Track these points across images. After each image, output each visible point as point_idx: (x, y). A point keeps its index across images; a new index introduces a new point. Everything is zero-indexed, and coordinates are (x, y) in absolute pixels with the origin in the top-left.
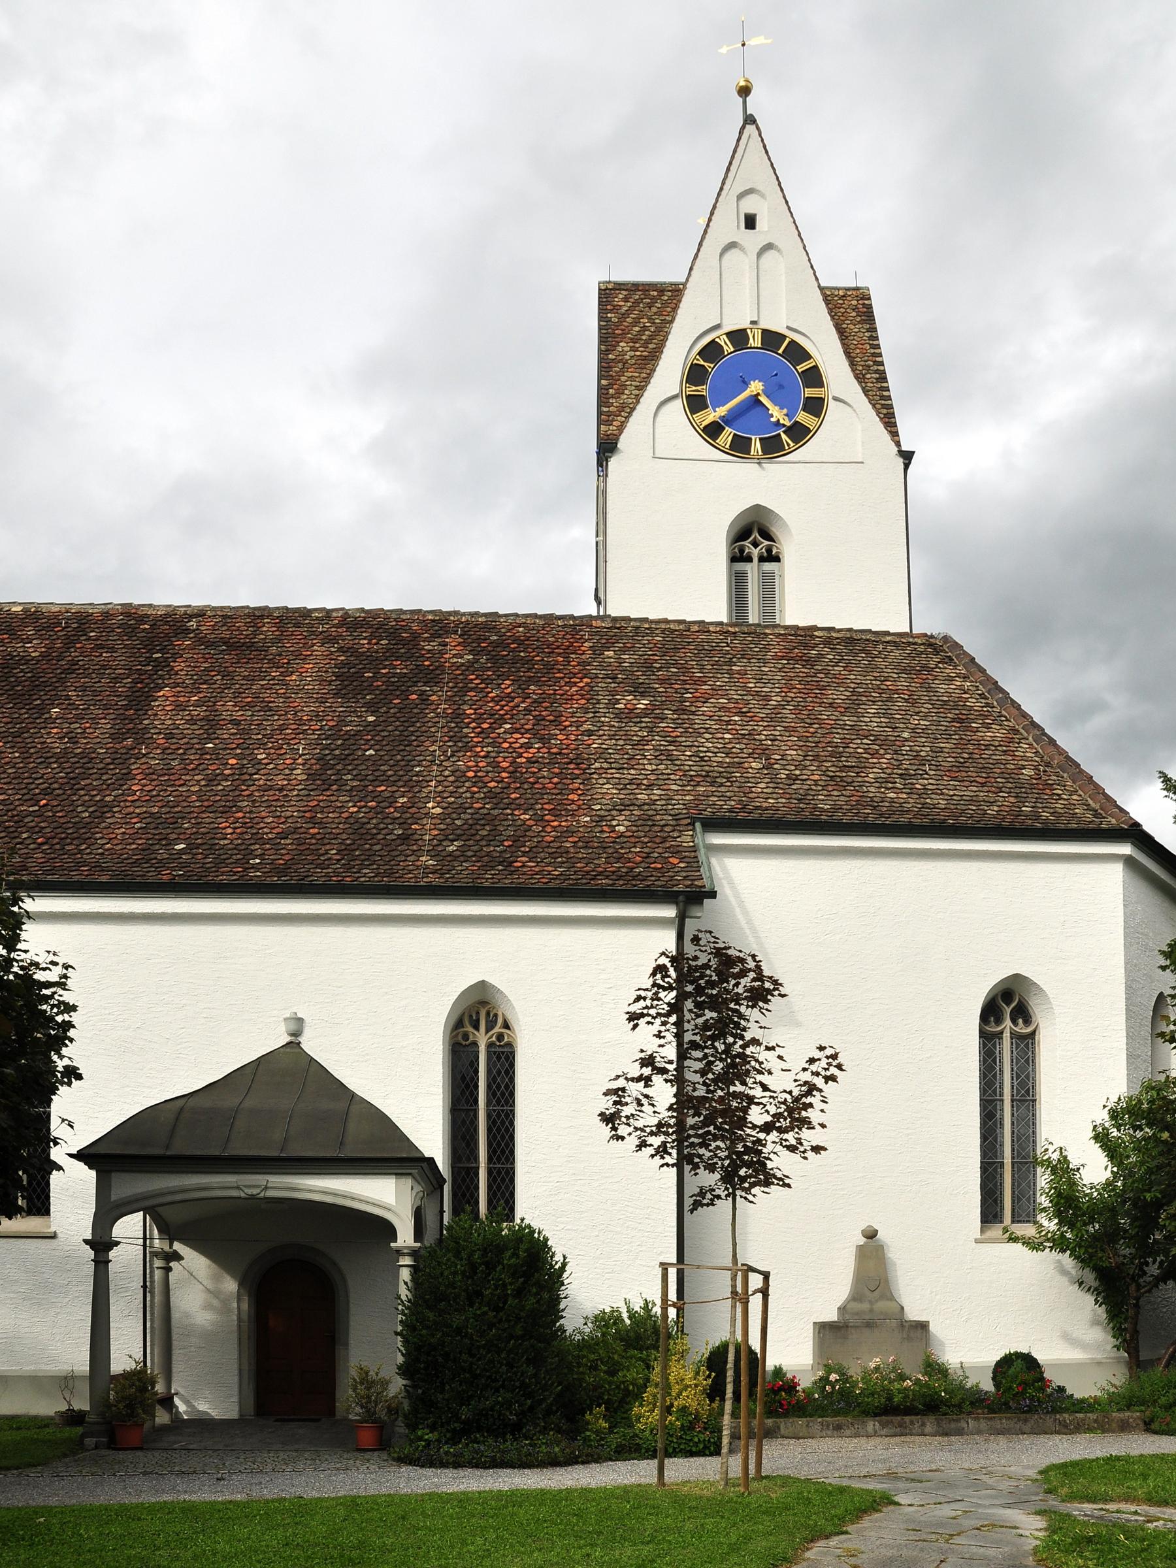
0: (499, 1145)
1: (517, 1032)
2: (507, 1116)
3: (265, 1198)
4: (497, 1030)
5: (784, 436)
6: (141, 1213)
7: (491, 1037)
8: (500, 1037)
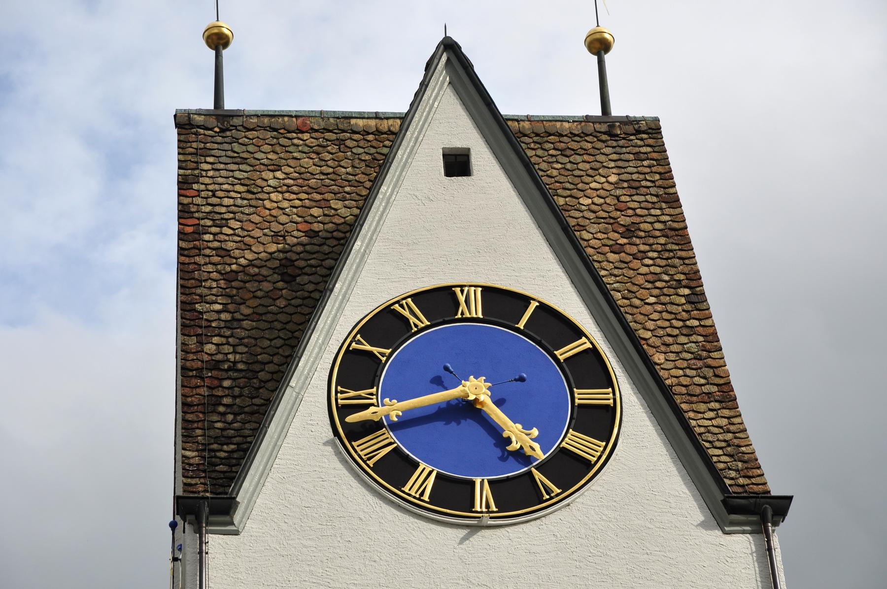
5: (538, 475)
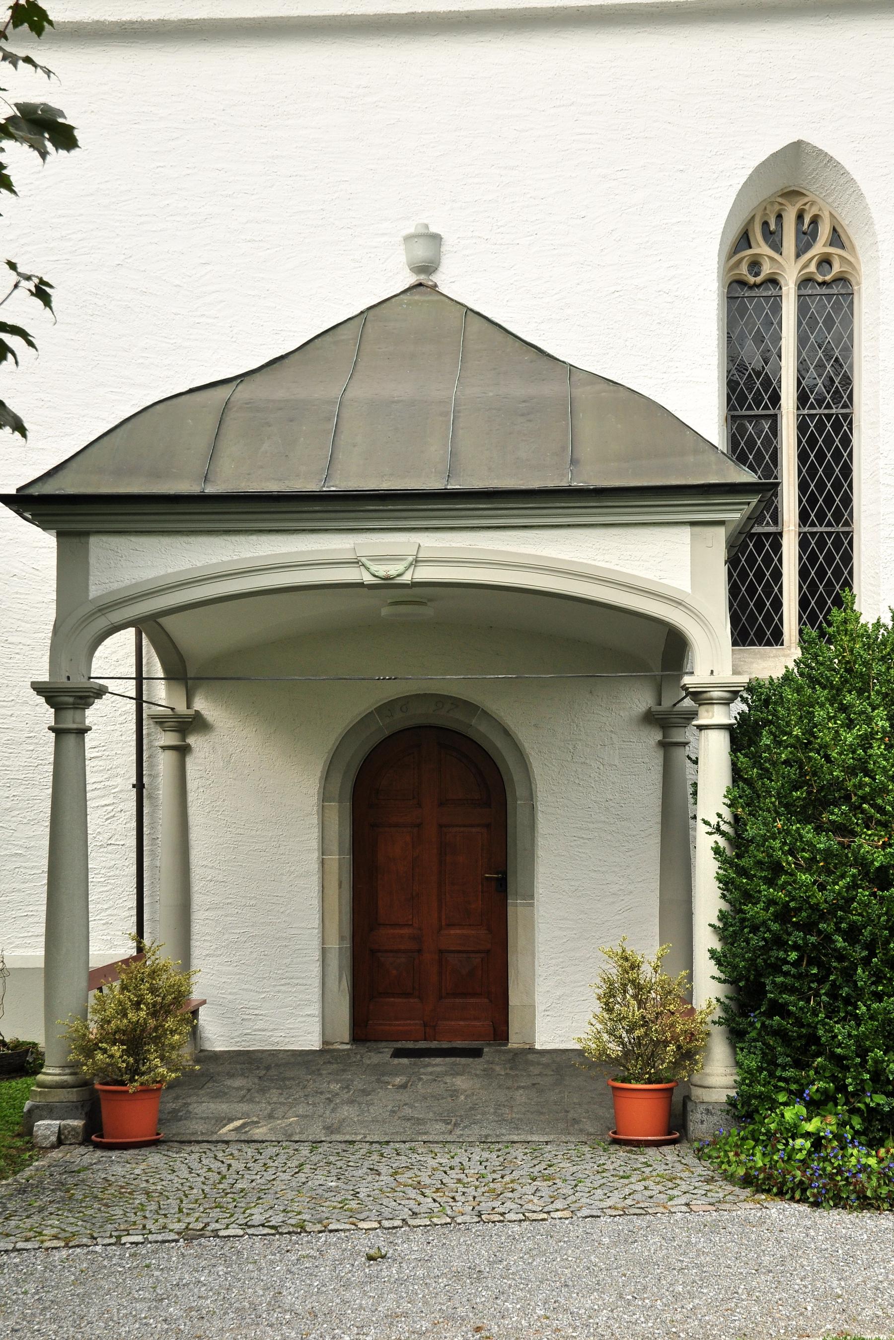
0: (821, 486)
1: (860, 251)
2: (837, 426)
3: (415, 585)
4: (819, 248)
6: (131, 632)
7: (806, 266)
8: (825, 262)
